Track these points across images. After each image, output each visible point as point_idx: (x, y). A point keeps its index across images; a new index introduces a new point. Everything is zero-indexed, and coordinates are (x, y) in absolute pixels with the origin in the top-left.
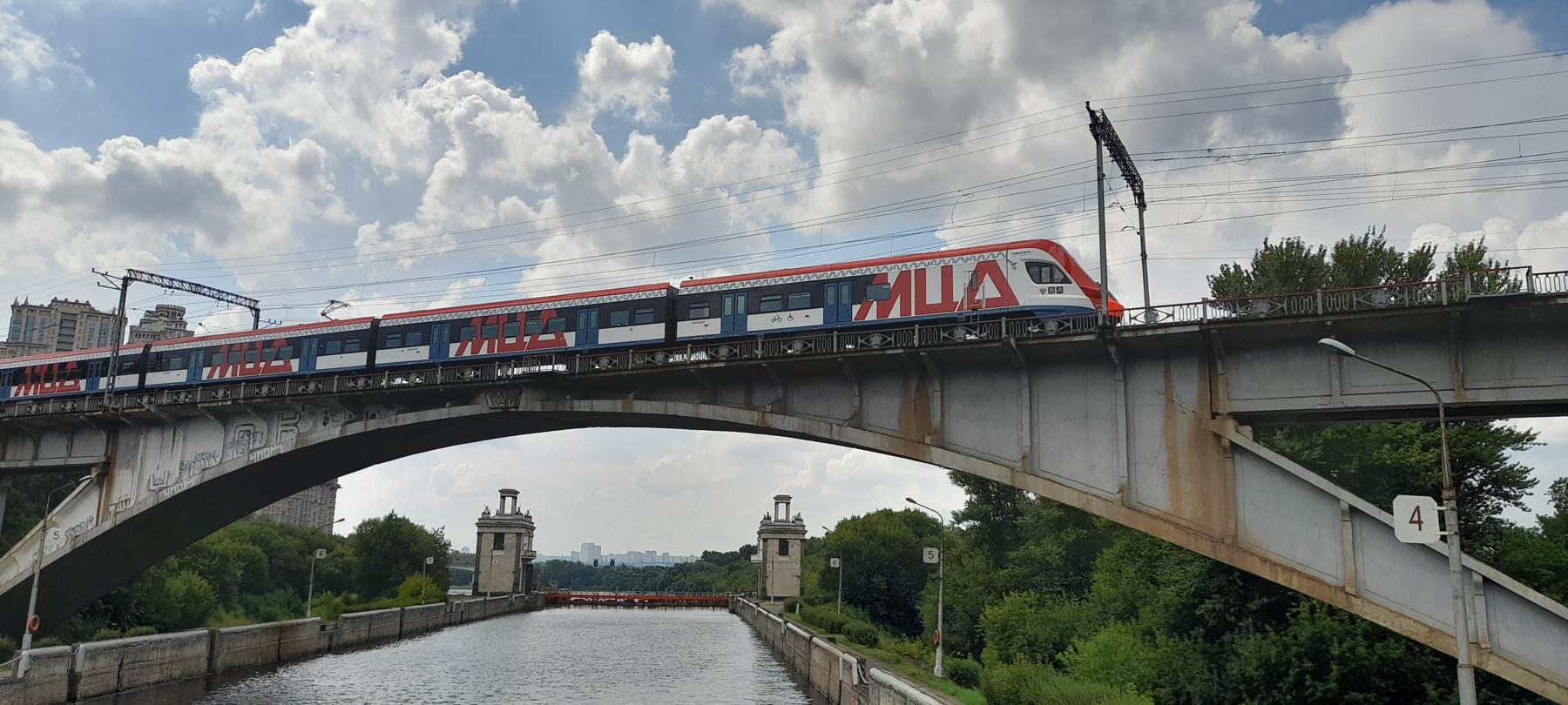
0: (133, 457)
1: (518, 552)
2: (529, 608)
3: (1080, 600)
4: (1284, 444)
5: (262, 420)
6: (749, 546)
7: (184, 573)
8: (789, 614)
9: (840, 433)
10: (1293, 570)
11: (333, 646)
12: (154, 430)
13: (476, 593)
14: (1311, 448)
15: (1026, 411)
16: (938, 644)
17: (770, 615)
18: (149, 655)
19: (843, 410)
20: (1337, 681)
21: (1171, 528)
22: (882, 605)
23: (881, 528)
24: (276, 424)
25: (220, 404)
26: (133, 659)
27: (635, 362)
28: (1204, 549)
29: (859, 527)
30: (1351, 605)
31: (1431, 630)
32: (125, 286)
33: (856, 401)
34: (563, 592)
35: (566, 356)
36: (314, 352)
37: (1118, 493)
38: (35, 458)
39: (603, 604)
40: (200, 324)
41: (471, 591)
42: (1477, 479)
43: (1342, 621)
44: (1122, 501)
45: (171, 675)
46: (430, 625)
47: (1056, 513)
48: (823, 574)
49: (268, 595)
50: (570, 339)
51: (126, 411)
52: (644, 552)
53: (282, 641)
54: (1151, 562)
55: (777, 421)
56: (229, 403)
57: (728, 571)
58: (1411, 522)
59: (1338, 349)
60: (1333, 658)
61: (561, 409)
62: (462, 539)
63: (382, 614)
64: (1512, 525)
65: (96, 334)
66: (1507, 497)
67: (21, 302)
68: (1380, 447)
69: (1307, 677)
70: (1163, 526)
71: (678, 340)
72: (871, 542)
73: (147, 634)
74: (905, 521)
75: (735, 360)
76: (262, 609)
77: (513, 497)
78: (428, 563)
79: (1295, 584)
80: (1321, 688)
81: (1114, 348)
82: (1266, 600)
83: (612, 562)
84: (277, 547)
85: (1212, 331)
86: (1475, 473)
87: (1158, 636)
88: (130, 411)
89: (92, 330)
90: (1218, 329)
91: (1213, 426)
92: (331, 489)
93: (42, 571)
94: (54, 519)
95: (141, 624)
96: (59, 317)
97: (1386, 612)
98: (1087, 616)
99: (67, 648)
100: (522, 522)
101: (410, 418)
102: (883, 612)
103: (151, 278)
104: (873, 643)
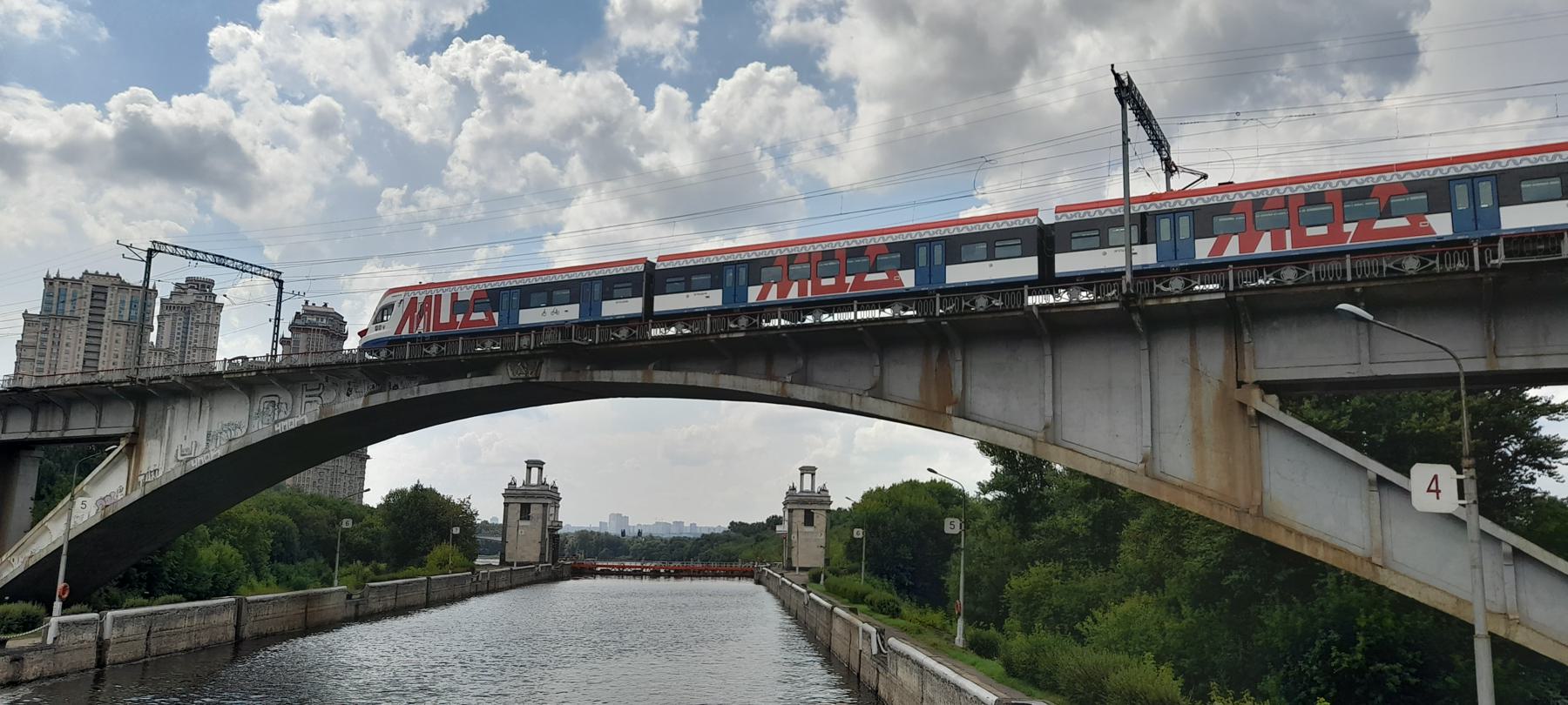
0: (161, 428)
1: (544, 522)
2: (556, 578)
3: (1106, 571)
4: (1312, 413)
6: (776, 516)
7: (215, 543)
9: (860, 403)
11: (360, 613)
13: (503, 563)
14: (1339, 417)
16: (959, 614)
17: (794, 585)
18: (177, 622)
20: (1363, 652)
21: (1196, 500)
22: (908, 576)
23: (906, 499)
24: (300, 395)
26: (160, 627)
27: (548, 338)
28: (1228, 518)
30: (1378, 575)
31: (1459, 600)
32: (149, 258)
33: (877, 371)
34: (589, 562)
35: (905, 297)
36: (515, 305)
37: (1141, 463)
38: (65, 429)
39: (628, 574)
40: (225, 296)
41: (498, 561)
42: (1512, 449)
44: (1146, 472)
45: (199, 643)
47: (1083, 483)
48: (849, 545)
50: (908, 279)
51: (153, 382)
52: (672, 523)
53: (309, 610)
55: (798, 391)
56: (253, 374)
58: (1429, 490)
59: (1353, 313)
62: (489, 509)
63: (409, 583)
64: (1546, 493)
65: (127, 306)
66: (1541, 467)
67: (53, 275)
70: (1187, 497)
71: (655, 314)
72: (897, 512)
73: (176, 602)
74: (930, 491)
77: (539, 468)
78: (454, 532)
79: (1321, 554)
80: (1347, 659)
81: (1138, 317)
82: (1292, 571)
85: (1238, 299)
86: (1510, 442)
87: (1183, 607)
88: (157, 382)
89: (123, 302)
90: (1245, 297)
91: (1238, 395)
93: (70, 542)
94: (84, 489)
95: (170, 593)
96: (90, 289)
97: (1414, 583)
98: (1114, 586)
99: (95, 615)
100: (548, 493)
101: (432, 389)
104: (895, 613)
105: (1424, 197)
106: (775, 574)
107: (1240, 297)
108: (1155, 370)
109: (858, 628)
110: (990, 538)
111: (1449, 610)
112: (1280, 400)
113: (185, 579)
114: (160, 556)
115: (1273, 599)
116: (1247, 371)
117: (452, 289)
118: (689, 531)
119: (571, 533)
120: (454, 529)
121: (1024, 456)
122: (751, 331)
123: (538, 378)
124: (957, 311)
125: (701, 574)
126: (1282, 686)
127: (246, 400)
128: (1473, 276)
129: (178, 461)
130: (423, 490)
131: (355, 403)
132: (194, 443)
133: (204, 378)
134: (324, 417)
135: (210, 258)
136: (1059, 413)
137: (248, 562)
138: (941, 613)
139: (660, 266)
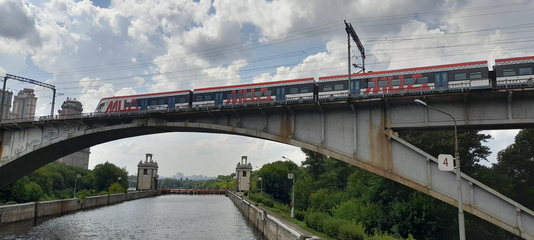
2: (155, 195)
3: (343, 191)
5: (56, 129)
8: (245, 196)
10: (410, 181)
12: (17, 132)
13: (137, 189)
15: (323, 127)
16: (292, 206)
17: (238, 197)
19: (261, 126)
21: (371, 167)
22: (278, 193)
23: (277, 168)
24: (61, 130)
25: (40, 123)
28: (381, 174)
29: (270, 167)
30: (429, 192)
31: (455, 201)
33: (266, 123)
34: (168, 189)
41: (136, 189)
43: (427, 198)
46: (119, 200)
47: (335, 162)
49: (64, 190)
51: (6, 125)
53: (63, 206)
54: (366, 178)
55: (238, 130)
56: (43, 122)
57: (227, 182)
60: (424, 210)
61: (163, 125)
62: (132, 171)
63: (101, 197)
66: (482, 157)
68: (441, 140)
69: (415, 216)
70: (368, 166)
73: (13, 204)
75: (224, 109)
76: (62, 195)
77: (151, 156)
78: (119, 179)
79: (411, 185)
82: (402, 191)
83: (187, 179)
84: (67, 174)
87: (367, 203)
88: (8, 125)
90: (388, 99)
91: (385, 132)
92: (87, 154)
97: (441, 195)
100: (154, 165)
102: (278, 195)
103: (15, 77)
104: (272, 206)
105: (427, 77)
106: (232, 193)
107: (386, 100)
108: (358, 124)
109: (258, 211)
110: (305, 180)
111: (452, 204)
112: (399, 134)
113: (20, 196)
114: (10, 187)
115: (396, 200)
116: (388, 125)
117: (125, 99)
118: (204, 179)
119: (163, 179)
120: (119, 178)
121: (316, 153)
122: (223, 109)
123: (147, 125)
124: (293, 103)
125: (207, 193)
126: (398, 229)
127: (41, 133)
128: (461, 93)
129: (16, 153)
130: (109, 164)
131: (81, 133)
132: (22, 147)
133: (25, 123)
134: (69, 138)
135: (28, 81)
136: (326, 138)
137: (44, 190)
138: (287, 205)
139: (195, 93)
